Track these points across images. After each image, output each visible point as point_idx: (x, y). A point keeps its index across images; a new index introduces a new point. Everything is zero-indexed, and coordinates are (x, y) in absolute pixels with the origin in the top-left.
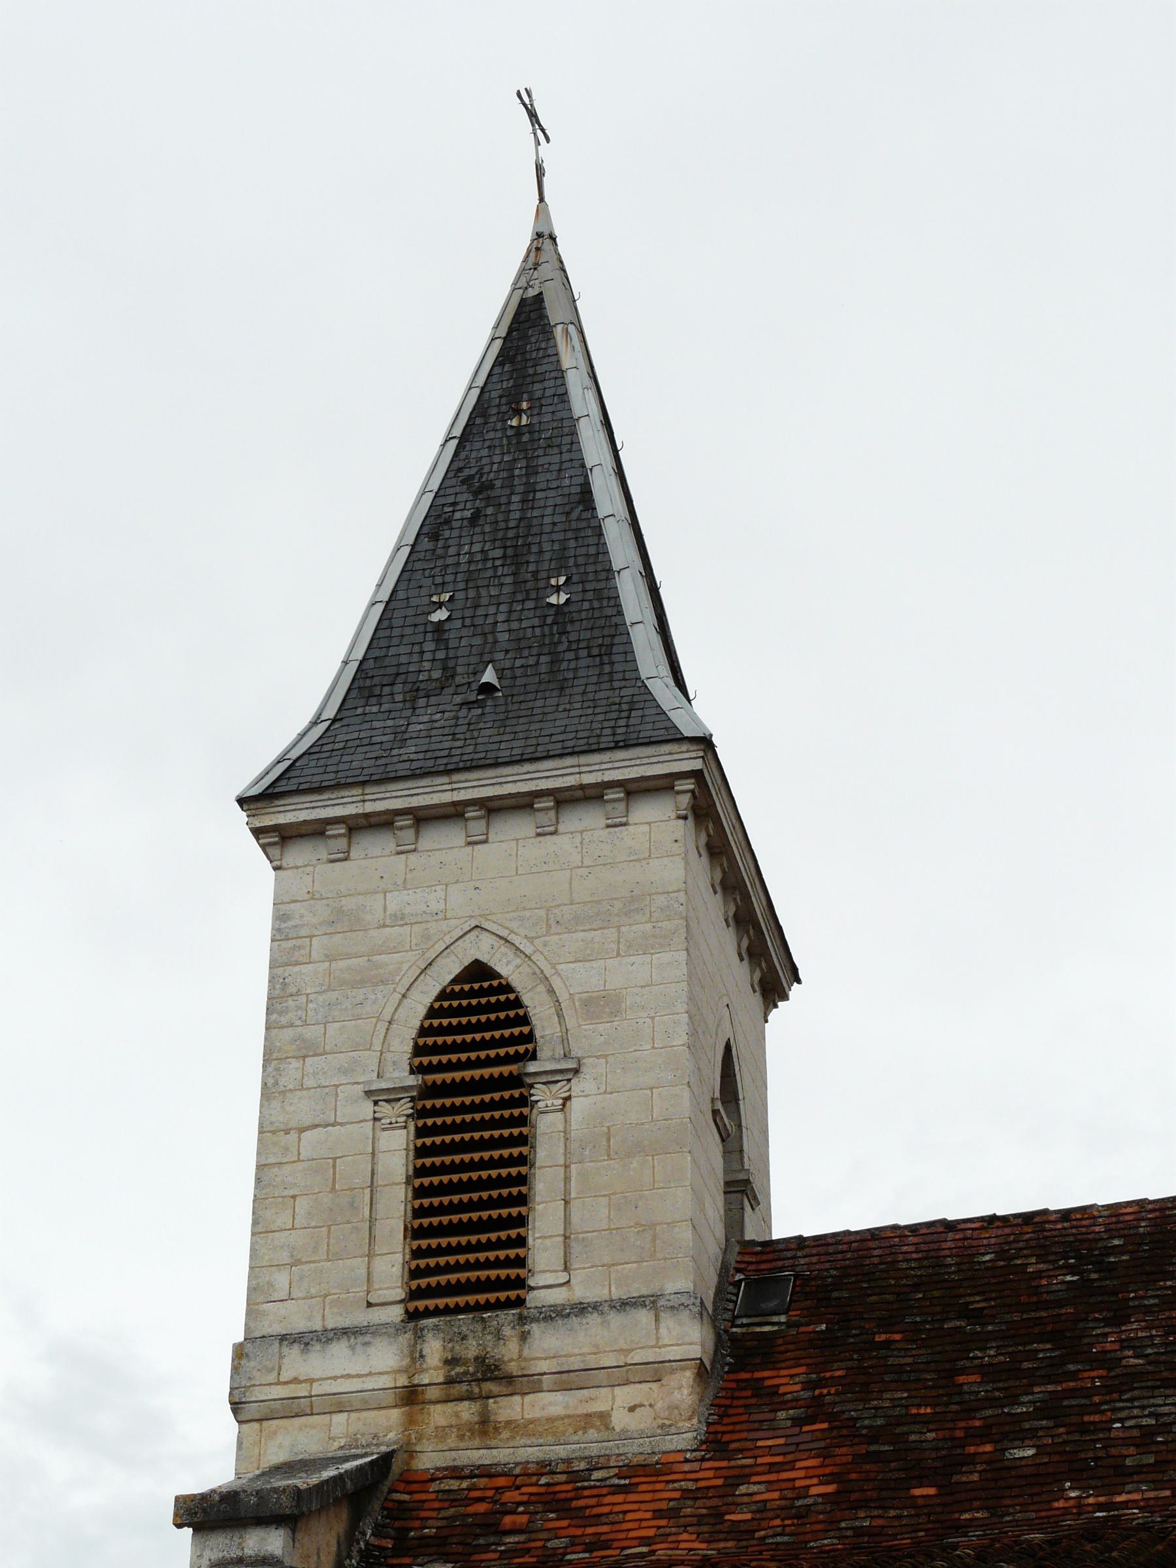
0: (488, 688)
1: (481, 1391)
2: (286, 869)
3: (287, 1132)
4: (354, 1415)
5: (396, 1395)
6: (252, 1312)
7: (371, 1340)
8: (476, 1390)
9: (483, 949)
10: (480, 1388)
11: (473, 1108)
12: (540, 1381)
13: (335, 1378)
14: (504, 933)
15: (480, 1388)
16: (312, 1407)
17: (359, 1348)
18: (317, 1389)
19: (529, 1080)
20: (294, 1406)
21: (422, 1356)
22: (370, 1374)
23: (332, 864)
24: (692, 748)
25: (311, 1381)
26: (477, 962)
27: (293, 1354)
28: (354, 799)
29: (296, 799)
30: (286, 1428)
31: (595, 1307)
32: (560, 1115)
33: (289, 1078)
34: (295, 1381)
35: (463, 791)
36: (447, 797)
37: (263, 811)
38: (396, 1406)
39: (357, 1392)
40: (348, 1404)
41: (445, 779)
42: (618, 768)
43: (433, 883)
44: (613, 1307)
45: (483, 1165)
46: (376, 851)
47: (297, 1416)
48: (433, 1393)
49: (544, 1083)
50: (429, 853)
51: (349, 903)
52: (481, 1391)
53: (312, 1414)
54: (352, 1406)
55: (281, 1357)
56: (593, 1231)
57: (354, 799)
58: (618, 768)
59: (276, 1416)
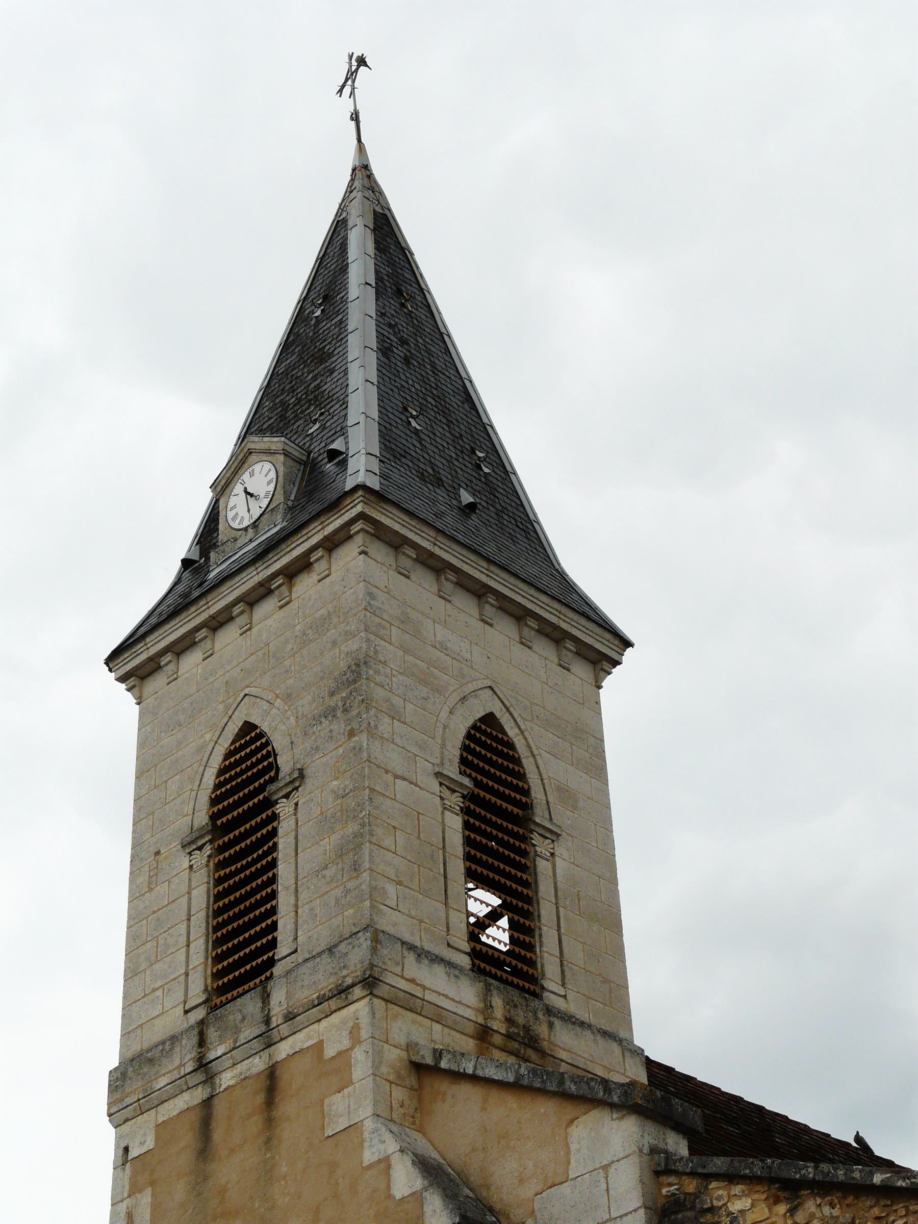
0: (472, 507)
1: (525, 1054)
2: (369, 557)
3: (387, 772)
4: (446, 1030)
5: (475, 1028)
6: (126, 1034)
7: (460, 976)
8: (523, 1052)
9: (496, 708)
10: (525, 1051)
11: (243, 868)
12: (560, 1065)
13: (439, 994)
14: (508, 704)
15: (525, 1051)
16: (422, 1008)
17: (453, 979)
18: (429, 996)
19: (533, 827)
20: (412, 1001)
21: (491, 1006)
22: (460, 1002)
23: (399, 575)
24: (620, 646)
25: (424, 988)
26: (492, 712)
27: (411, 958)
28: (429, 538)
29: (395, 511)
30: (403, 1017)
31: (590, 1026)
32: (397, 830)
33: (111, 666)
34: (412, 981)
35: (493, 581)
36: (144, 656)
37: (373, 505)
38: (472, 1037)
39: (452, 1012)
40: (444, 1019)
41: (485, 564)
42: (579, 630)
43: (462, 635)
44: (599, 1031)
45: (497, 870)
46: (426, 585)
47: (411, 1010)
48: (497, 1039)
49: (539, 834)
50: (460, 611)
51: (413, 614)
52: (525, 1054)
53: (420, 1014)
54: (446, 1021)
55: (404, 957)
56: (577, 966)
57: (429, 538)
58: (579, 630)
59: (398, 1003)
